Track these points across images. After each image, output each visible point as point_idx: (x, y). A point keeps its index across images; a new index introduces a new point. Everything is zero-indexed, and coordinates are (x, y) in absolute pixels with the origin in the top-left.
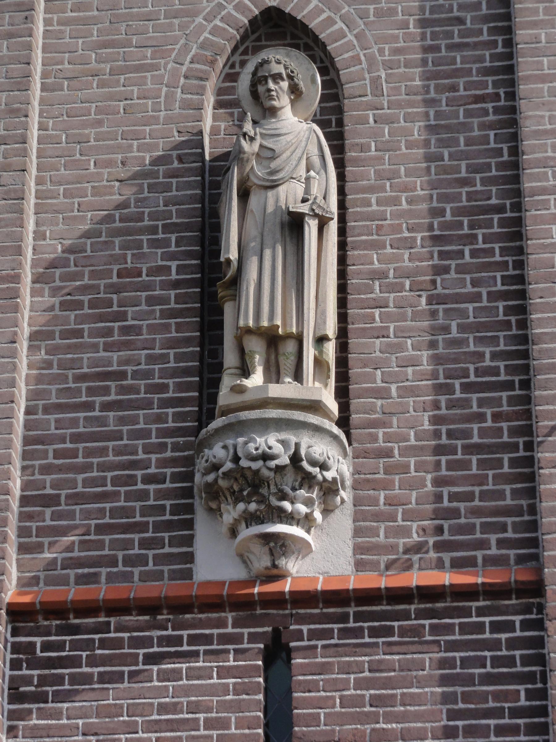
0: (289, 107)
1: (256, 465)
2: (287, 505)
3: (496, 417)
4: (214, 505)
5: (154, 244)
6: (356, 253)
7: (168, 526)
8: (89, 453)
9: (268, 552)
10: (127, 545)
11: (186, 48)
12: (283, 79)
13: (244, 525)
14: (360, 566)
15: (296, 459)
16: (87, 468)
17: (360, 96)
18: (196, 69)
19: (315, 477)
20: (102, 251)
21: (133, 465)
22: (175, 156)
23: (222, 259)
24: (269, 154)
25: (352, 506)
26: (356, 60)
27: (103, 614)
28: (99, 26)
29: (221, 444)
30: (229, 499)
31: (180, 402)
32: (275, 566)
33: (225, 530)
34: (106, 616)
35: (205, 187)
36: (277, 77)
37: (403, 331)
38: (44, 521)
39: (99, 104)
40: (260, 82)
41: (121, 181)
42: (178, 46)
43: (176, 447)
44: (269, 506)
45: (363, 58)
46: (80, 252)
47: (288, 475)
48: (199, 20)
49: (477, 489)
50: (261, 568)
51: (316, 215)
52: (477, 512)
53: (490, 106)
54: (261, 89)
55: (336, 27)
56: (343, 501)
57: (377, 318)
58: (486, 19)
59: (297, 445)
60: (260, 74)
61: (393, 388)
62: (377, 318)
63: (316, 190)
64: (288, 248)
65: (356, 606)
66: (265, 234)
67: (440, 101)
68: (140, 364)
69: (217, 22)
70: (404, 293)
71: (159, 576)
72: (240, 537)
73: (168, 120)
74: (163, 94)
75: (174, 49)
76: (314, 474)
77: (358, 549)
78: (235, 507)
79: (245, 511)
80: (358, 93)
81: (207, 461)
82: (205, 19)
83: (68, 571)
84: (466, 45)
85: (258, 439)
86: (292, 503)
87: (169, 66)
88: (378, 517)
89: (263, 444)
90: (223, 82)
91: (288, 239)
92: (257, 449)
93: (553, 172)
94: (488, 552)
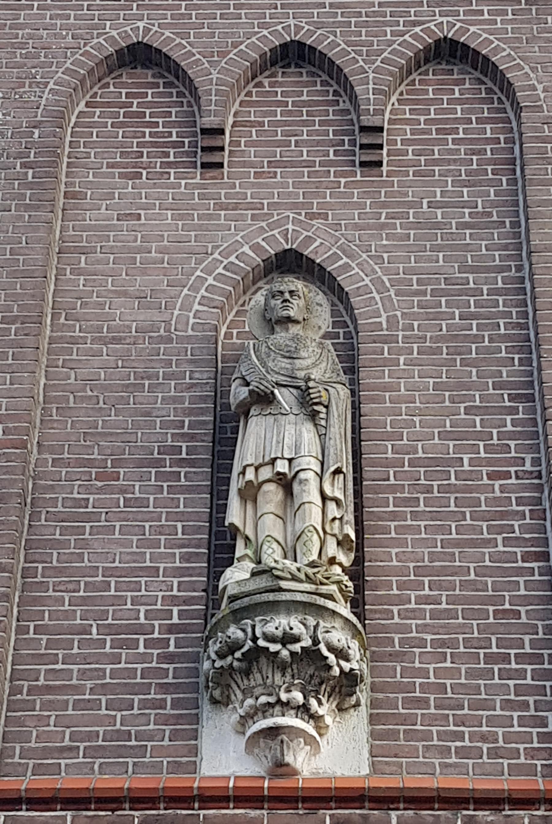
19: (330, 667)
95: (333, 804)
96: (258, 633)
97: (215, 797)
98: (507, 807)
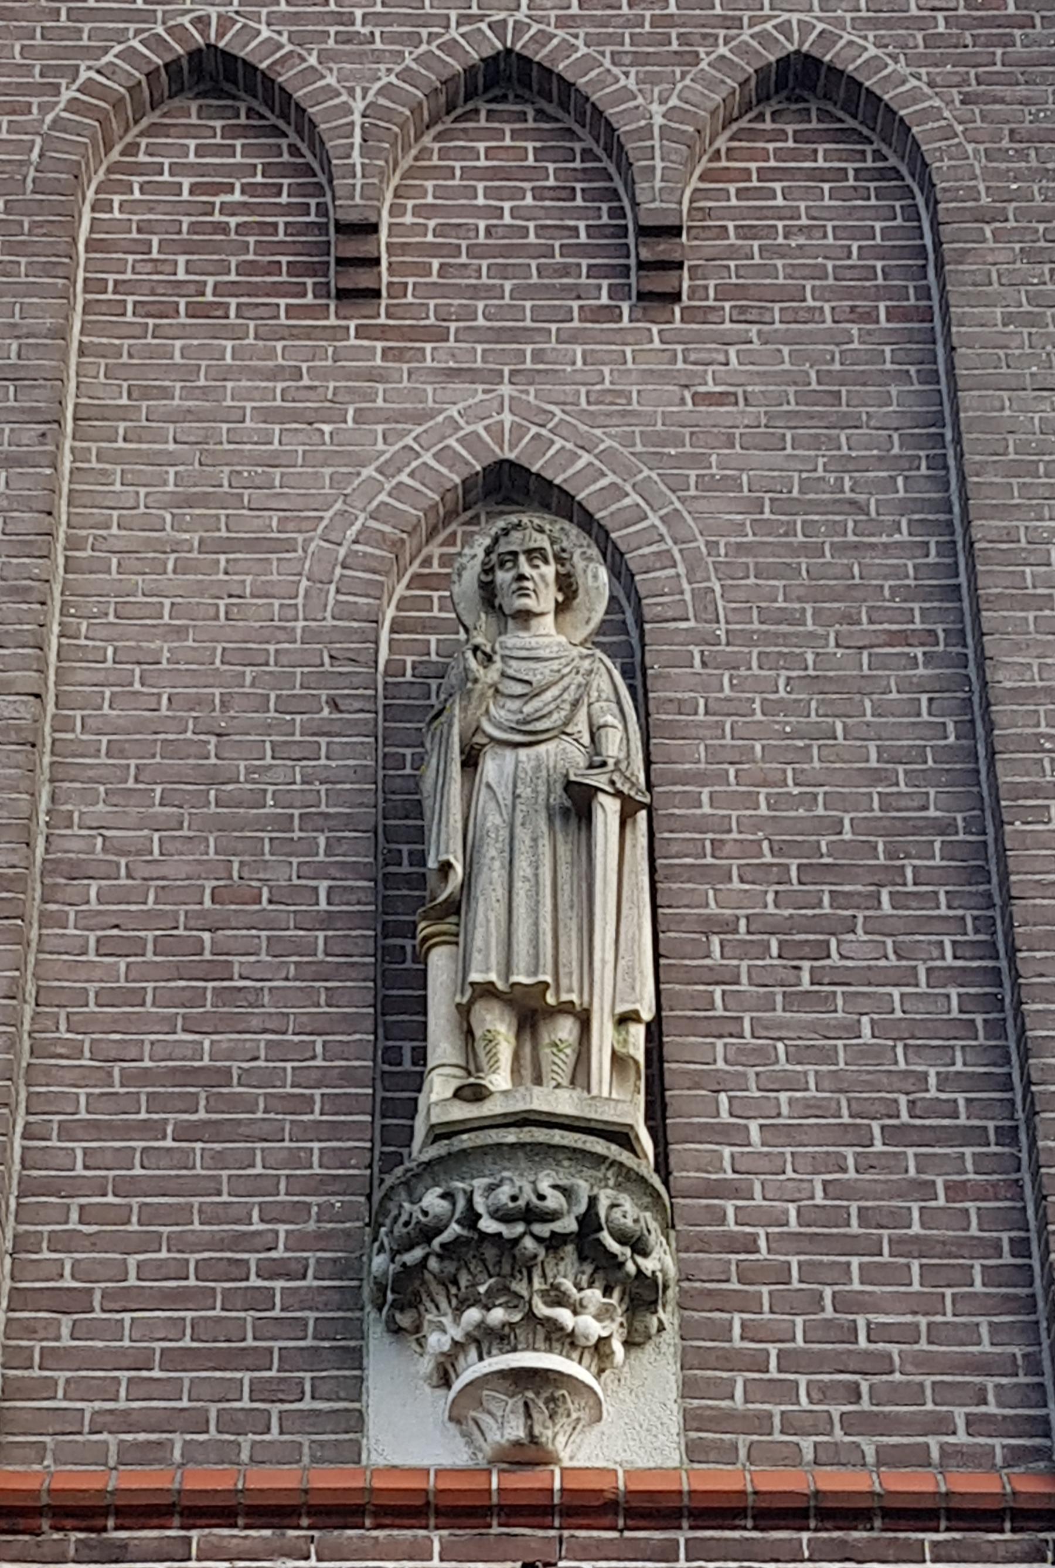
0: (550, 619)
1: (510, 1231)
2: (564, 1316)
3: (954, 1190)
4: (404, 1320)
5: (284, 847)
6: (675, 886)
7: (312, 1358)
8: (149, 1215)
9: (521, 1409)
10: (229, 1392)
11: (345, 517)
12: (546, 562)
13: (473, 1354)
14: (694, 1452)
15: (589, 1221)
16: (152, 1242)
17: (675, 620)
18: (365, 554)
20: (181, 854)
21: (238, 1241)
22: (324, 698)
23: (432, 864)
24: (519, 689)
25: (678, 1340)
26: (666, 560)
27: (176, 1521)
28: (181, 468)
29: (439, 1191)
30: (444, 1305)
31: (335, 1131)
32: (533, 1439)
33: (426, 1365)
34: (182, 1527)
35: (412, 720)
36: (534, 554)
37: (766, 1028)
38: (58, 1338)
39: (179, 600)
40: (502, 564)
41: (218, 735)
42: (330, 513)
43: (325, 1213)
44: (530, 1315)
45: (677, 556)
46: (138, 853)
47: (568, 1260)
48: (369, 471)
49: (923, 1321)
50: (503, 1441)
51: (618, 794)
52: (925, 1363)
53: (919, 652)
54: (503, 577)
55: (627, 501)
56: (661, 1328)
57: (718, 1002)
58: (904, 507)
59: (593, 1201)
60: (502, 548)
61: (754, 1126)
62: (718, 1002)
63: (612, 746)
64: (563, 850)
65: (692, 1528)
66: (518, 821)
67: (826, 637)
68: (256, 1059)
69: (404, 477)
70: (768, 962)
71: (291, 1455)
72: (458, 1385)
73: (309, 635)
74: (302, 592)
75: (322, 518)
76: (621, 1259)
77: (691, 1420)
78: (457, 1320)
79: (481, 1325)
80: (670, 614)
81: (406, 1224)
82: (381, 473)
83: (104, 1436)
84: (873, 546)
85: (518, 1184)
86: (575, 1313)
87: (312, 547)
88: (730, 1361)
89: (528, 1189)
90: (408, 587)
91: (560, 837)
92: (514, 1198)
93: (1052, 760)
94: (951, 1439)
95: (176, 1521)
96: (480, 1207)
97: (408, 1508)
98: (495, 1522)
